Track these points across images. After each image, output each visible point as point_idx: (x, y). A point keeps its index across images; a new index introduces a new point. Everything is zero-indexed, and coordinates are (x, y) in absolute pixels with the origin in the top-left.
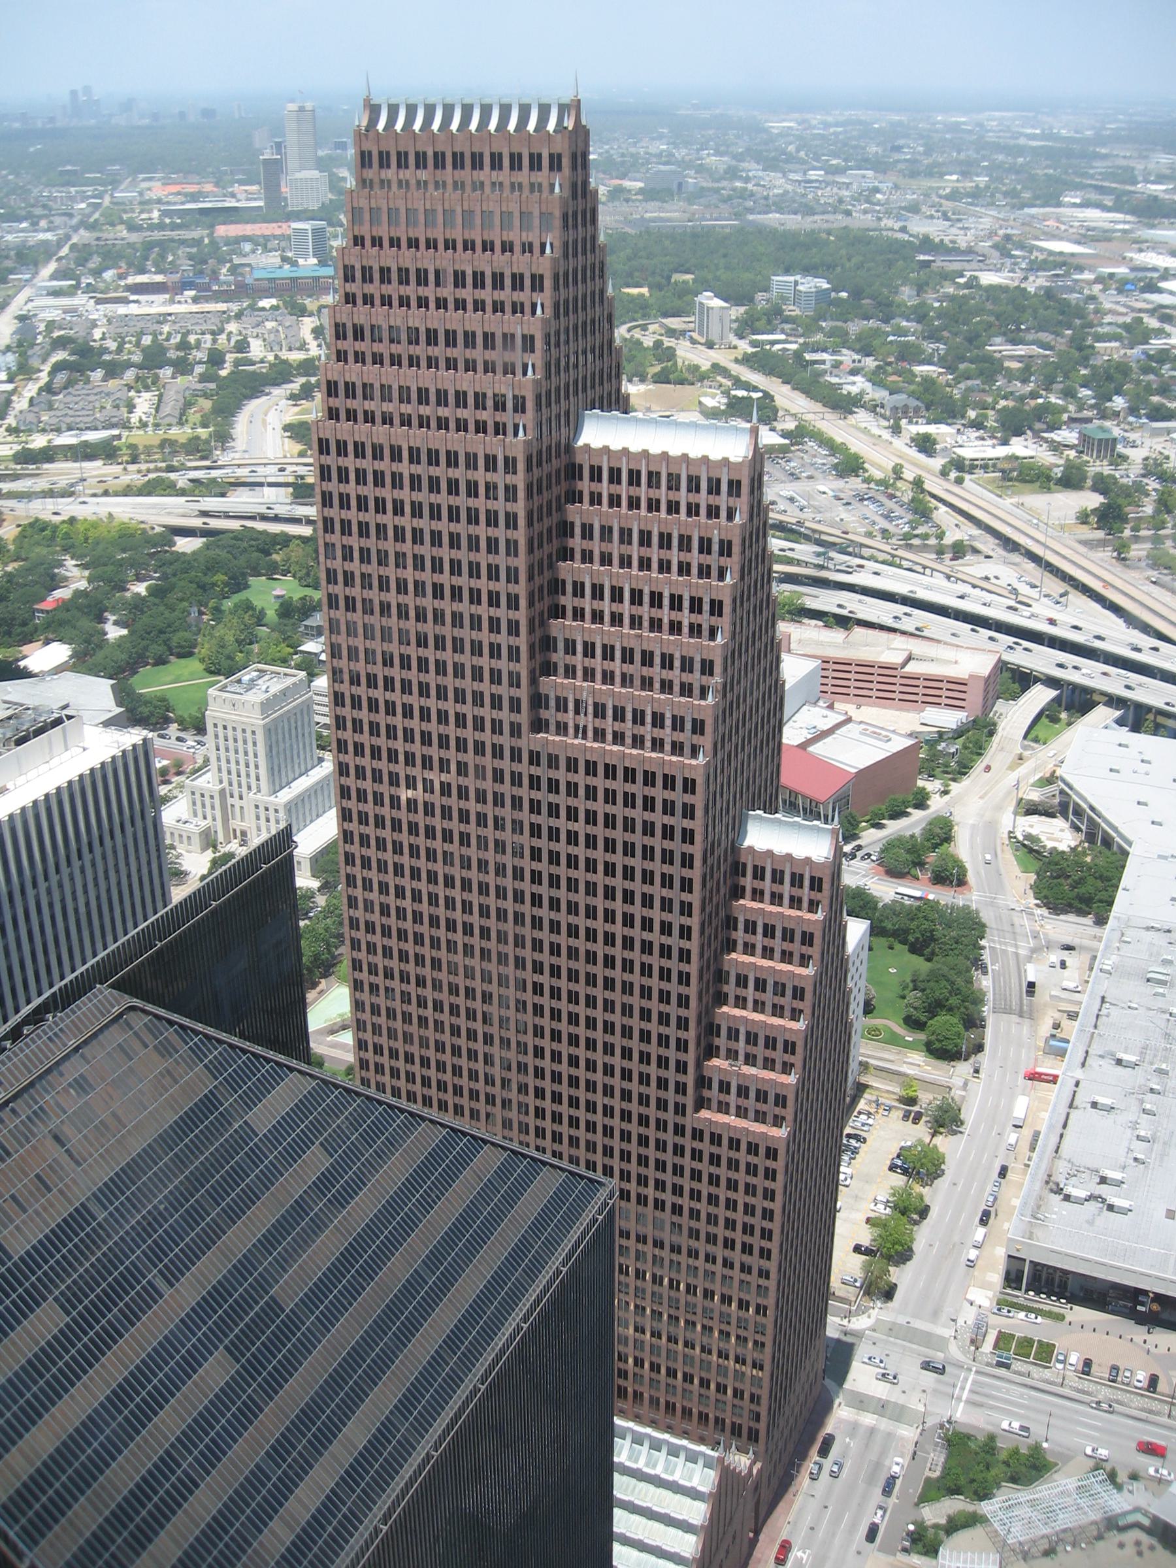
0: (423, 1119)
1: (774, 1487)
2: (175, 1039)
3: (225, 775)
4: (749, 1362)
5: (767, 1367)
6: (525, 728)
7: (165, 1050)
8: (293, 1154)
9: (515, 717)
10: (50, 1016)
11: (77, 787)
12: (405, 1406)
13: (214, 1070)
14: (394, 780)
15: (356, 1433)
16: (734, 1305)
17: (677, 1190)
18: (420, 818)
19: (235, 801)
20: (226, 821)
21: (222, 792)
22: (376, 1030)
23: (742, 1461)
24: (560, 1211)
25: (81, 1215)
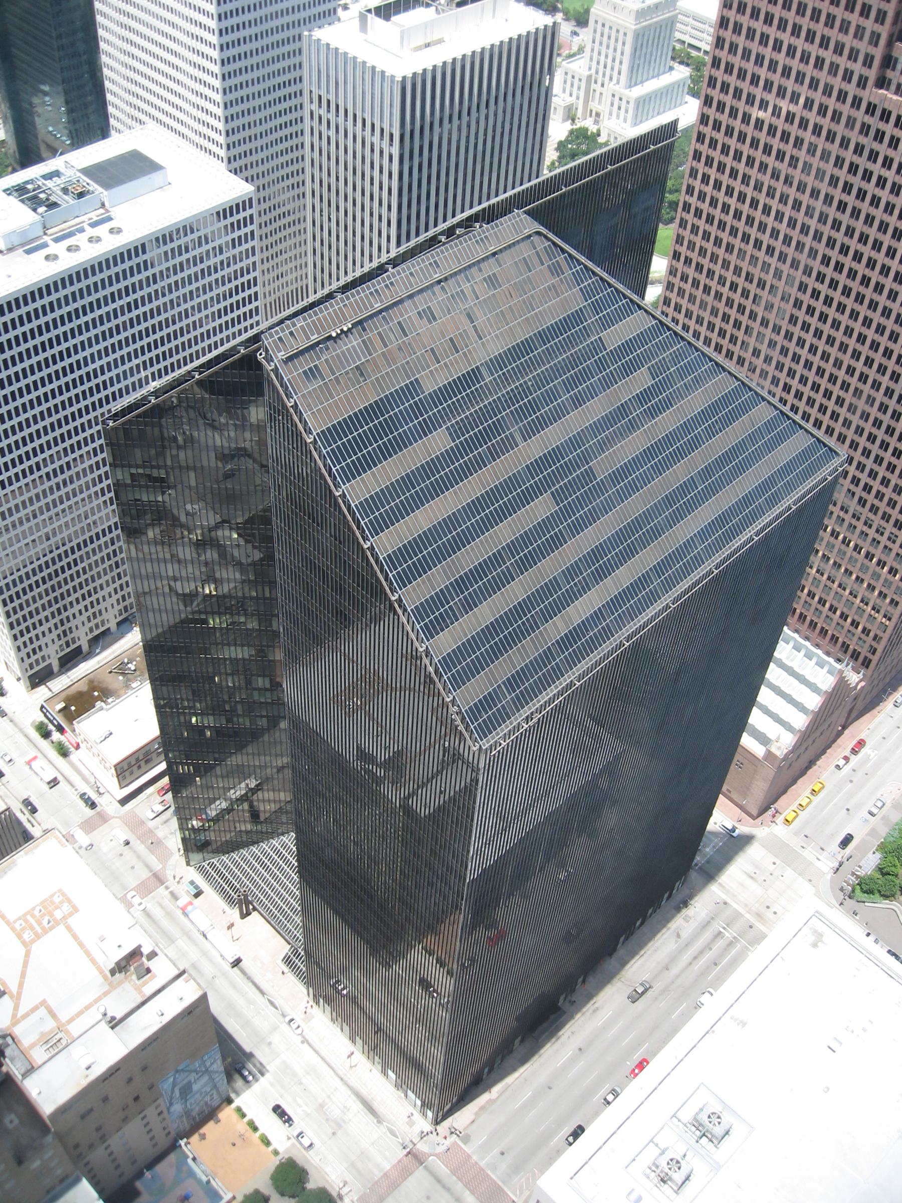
0: (724, 370)
1: (869, 701)
2: (564, 264)
3: (594, 63)
4: (882, 612)
5: (894, 620)
6: (870, 83)
7: (556, 270)
8: (628, 370)
9: (866, 72)
10: (477, 225)
11: (496, 50)
12: (659, 569)
13: (586, 293)
14: (751, 100)
15: (623, 576)
16: (886, 569)
17: (873, 474)
18: (763, 136)
19: (598, 87)
20: (586, 101)
21: (589, 77)
22: (681, 293)
23: (854, 678)
24: (804, 464)
25: (473, 376)
